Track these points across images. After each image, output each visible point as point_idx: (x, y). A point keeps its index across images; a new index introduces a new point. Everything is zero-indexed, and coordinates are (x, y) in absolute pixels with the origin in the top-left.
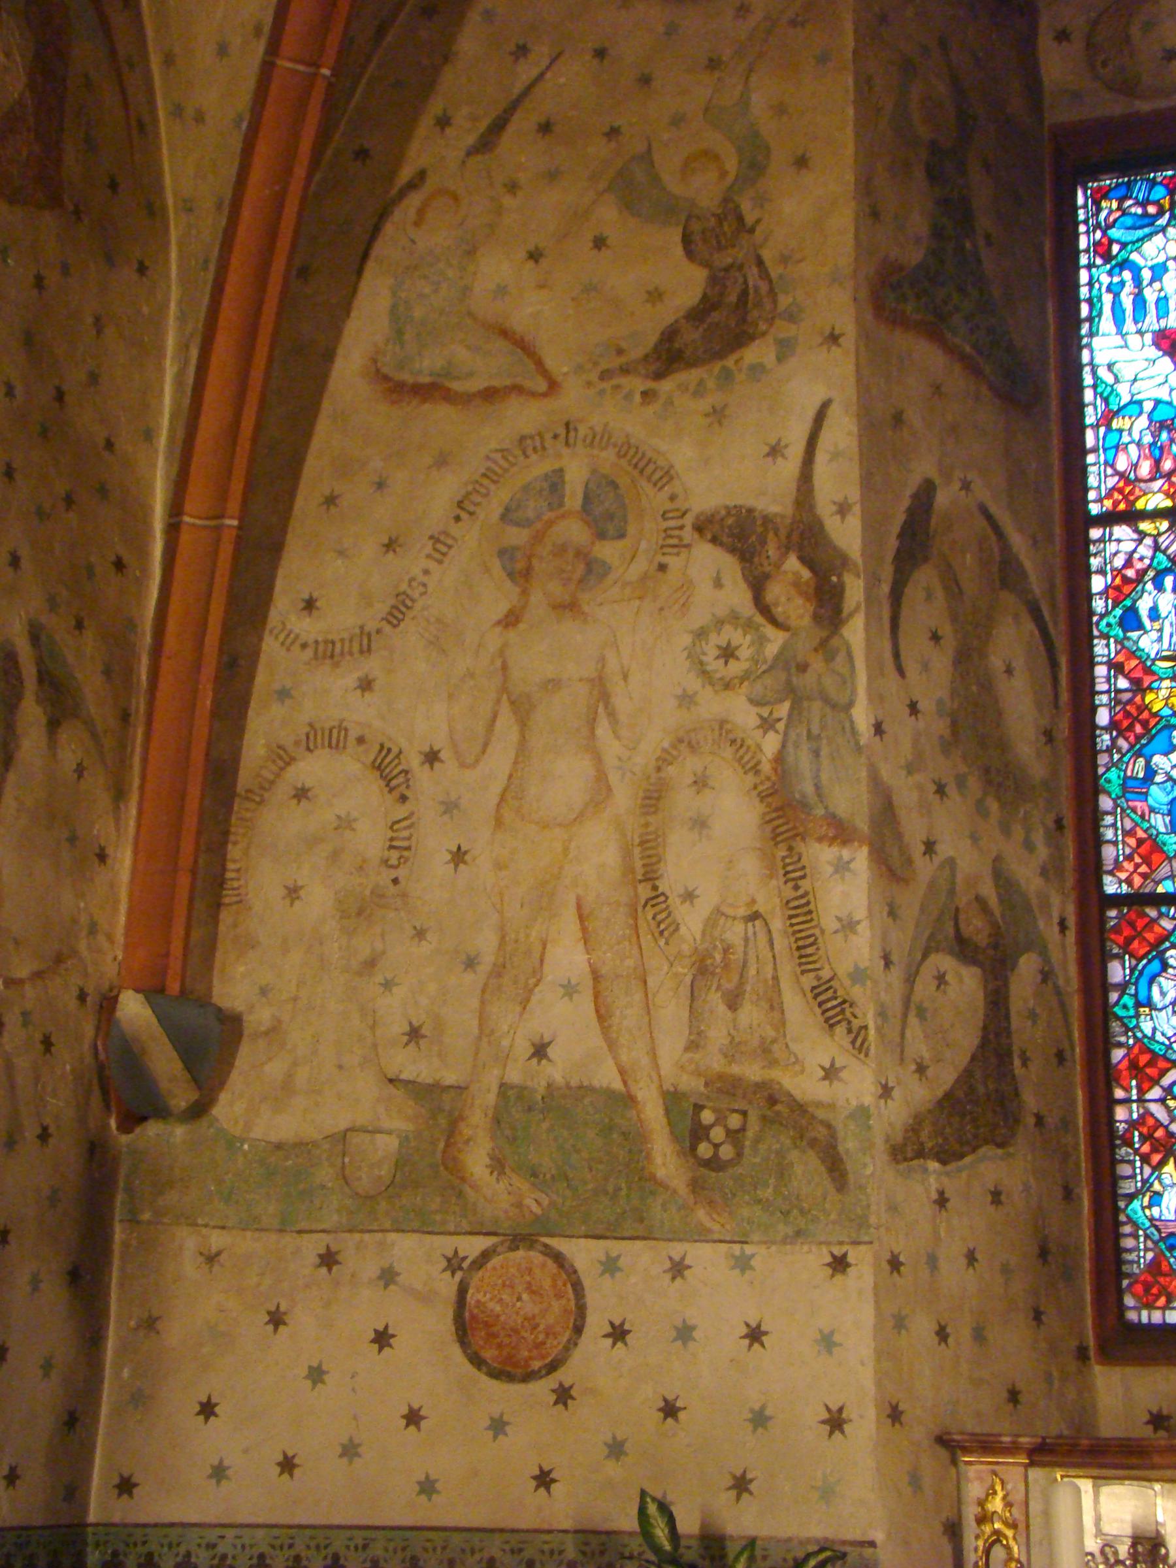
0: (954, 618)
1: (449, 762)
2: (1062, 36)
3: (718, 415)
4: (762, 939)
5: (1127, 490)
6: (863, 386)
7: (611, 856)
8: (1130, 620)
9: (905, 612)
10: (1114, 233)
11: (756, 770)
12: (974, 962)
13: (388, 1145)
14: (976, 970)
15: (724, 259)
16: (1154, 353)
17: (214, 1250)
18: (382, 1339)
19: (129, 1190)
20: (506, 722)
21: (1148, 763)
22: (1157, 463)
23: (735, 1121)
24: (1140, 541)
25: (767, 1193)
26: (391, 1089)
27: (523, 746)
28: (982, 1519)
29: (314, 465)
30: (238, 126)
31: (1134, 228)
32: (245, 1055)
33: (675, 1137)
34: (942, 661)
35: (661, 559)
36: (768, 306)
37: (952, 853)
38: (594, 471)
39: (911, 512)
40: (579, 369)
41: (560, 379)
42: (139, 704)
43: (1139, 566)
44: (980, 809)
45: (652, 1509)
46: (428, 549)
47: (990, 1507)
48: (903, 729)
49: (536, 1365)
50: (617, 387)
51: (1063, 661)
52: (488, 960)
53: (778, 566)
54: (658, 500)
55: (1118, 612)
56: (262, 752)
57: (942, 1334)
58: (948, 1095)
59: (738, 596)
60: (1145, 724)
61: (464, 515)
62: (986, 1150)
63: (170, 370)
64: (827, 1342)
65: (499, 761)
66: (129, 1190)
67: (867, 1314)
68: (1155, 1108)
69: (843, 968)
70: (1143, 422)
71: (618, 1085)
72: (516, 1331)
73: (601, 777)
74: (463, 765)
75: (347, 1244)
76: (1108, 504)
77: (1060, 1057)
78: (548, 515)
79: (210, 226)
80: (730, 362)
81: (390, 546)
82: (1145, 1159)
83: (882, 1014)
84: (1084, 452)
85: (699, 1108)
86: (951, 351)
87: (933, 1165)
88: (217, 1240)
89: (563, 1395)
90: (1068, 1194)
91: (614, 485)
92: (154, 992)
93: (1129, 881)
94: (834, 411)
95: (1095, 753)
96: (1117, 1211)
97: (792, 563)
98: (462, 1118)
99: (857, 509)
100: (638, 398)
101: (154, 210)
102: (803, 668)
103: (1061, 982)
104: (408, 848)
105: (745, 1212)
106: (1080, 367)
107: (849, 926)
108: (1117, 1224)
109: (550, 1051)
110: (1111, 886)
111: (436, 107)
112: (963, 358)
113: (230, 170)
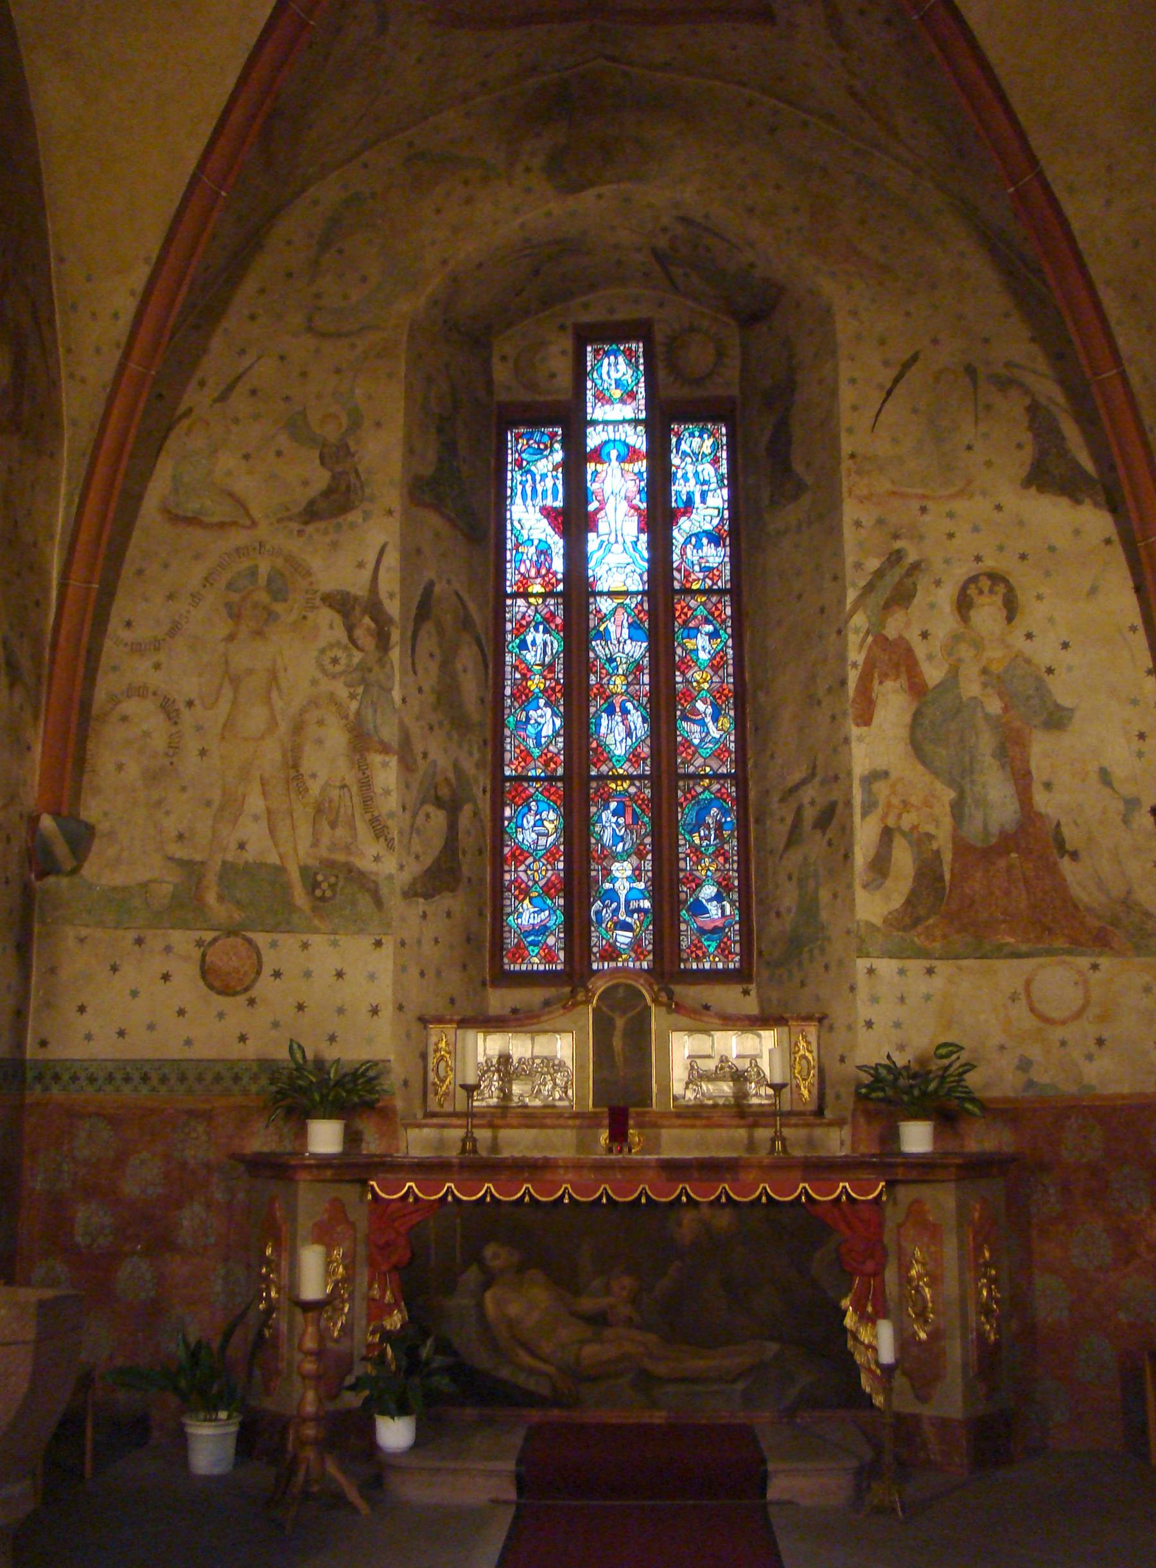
2: (504, 358)
3: (335, 545)
4: (347, 795)
5: (525, 581)
6: (403, 536)
7: (278, 756)
8: (523, 646)
10: (524, 456)
13: (168, 888)
14: (444, 812)
15: (339, 469)
16: (539, 516)
17: (83, 936)
21: (527, 715)
22: (538, 571)
23: (333, 880)
24: (529, 608)
25: (347, 912)
27: (235, 702)
28: (436, 1051)
29: (132, 552)
31: (533, 454)
32: (97, 845)
33: (304, 886)
34: (434, 667)
35: (304, 613)
36: (360, 493)
38: (273, 567)
42: (46, 671)
43: (528, 619)
44: (450, 737)
46: (190, 600)
47: (440, 1046)
49: (239, 989)
51: (491, 666)
52: (216, 804)
53: (360, 621)
55: (517, 641)
56: (104, 696)
57: (422, 974)
59: (340, 634)
60: (527, 696)
61: (208, 585)
63: (62, 504)
64: (372, 977)
65: (224, 706)
67: (390, 966)
69: (384, 810)
70: (532, 550)
71: (278, 862)
72: (229, 974)
73: (273, 717)
76: (515, 588)
77: (480, 852)
80: (340, 520)
82: (516, 897)
83: (401, 833)
84: (506, 562)
85: (316, 874)
86: (442, 514)
87: (421, 900)
88: (84, 932)
89: (252, 1002)
91: (283, 575)
92: (56, 814)
93: (516, 770)
94: (389, 548)
95: (503, 708)
96: (502, 921)
97: (367, 620)
98: (204, 876)
99: (398, 596)
101: (58, 425)
103: (482, 817)
104: (177, 748)
105: (336, 921)
106: (506, 520)
107: (387, 792)
108: (503, 926)
109: (247, 847)
110: (507, 773)
111: (199, 375)
112: (449, 520)
113: (99, 410)
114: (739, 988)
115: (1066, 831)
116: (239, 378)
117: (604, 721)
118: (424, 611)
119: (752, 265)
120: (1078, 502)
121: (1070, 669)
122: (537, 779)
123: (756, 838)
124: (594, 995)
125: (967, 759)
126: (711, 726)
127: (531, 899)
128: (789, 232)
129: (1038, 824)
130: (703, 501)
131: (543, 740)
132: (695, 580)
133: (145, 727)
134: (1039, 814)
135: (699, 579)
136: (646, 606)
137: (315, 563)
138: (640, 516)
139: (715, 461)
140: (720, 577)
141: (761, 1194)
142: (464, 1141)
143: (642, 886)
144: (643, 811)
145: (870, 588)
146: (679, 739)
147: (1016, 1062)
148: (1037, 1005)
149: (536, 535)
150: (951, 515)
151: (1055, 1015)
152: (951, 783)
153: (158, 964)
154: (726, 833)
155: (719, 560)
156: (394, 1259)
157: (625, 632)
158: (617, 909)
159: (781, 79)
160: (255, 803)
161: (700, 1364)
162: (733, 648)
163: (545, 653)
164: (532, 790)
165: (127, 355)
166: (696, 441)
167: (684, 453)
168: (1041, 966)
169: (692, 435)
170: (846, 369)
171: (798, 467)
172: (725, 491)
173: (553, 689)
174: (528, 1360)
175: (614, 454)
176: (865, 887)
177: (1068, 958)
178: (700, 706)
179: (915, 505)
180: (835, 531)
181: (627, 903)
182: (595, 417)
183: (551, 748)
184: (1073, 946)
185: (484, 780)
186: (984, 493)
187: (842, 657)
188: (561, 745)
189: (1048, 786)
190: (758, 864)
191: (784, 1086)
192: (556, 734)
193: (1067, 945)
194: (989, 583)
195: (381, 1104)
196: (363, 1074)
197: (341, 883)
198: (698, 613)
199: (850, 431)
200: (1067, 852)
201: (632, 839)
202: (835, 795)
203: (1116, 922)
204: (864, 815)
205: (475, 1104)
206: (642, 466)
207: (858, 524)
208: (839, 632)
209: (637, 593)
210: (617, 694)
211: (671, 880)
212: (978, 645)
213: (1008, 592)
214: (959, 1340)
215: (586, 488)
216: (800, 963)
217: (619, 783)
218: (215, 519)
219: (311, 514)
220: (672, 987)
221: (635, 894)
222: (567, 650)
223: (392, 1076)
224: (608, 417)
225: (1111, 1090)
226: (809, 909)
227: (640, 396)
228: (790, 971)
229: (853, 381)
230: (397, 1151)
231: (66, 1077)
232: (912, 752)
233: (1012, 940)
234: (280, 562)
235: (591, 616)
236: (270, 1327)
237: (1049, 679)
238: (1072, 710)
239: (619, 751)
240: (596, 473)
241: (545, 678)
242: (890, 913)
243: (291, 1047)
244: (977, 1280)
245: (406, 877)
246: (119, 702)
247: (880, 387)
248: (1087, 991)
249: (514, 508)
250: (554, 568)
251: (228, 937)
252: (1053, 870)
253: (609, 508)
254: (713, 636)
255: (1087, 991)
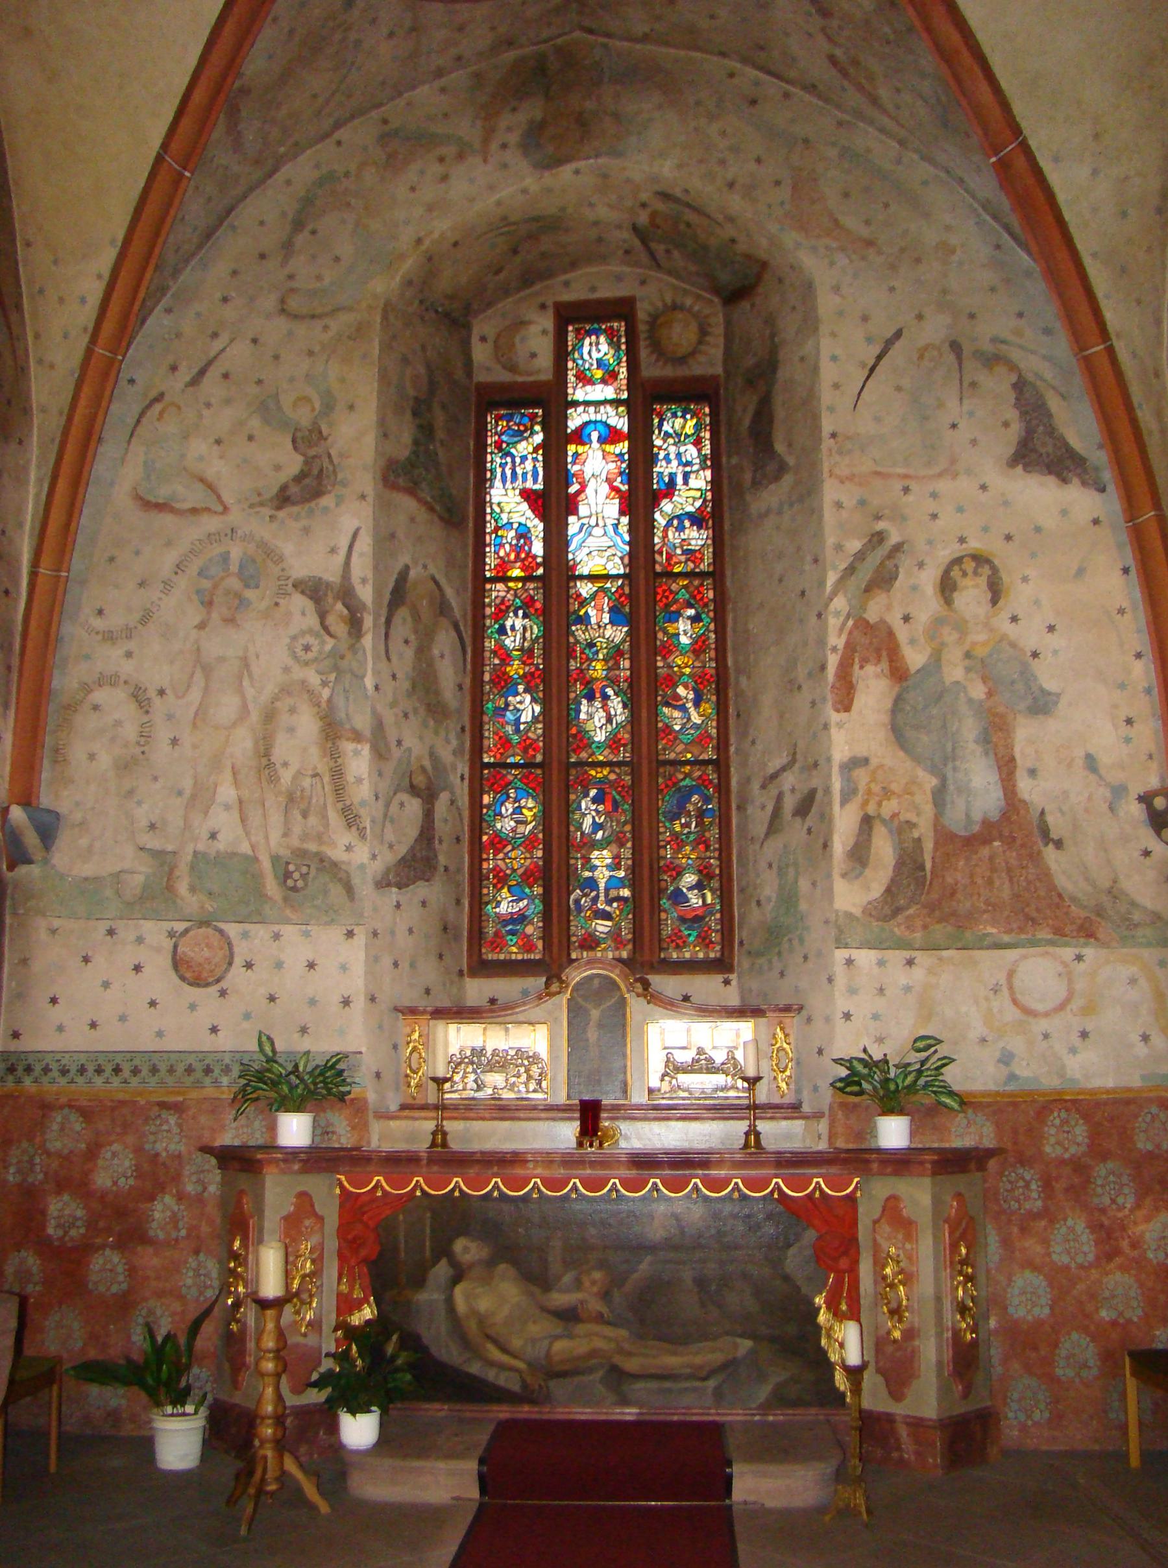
0: (416, 632)
1: (170, 696)
2: (483, 339)
3: (306, 530)
4: (319, 785)
7: (249, 744)
8: (502, 631)
9: (392, 632)
10: (504, 438)
11: (318, 705)
12: (418, 796)
13: (139, 879)
14: (419, 800)
15: (312, 452)
16: (519, 499)
18: (137, 968)
19: (13, 898)
20: (199, 676)
23: (304, 870)
24: (508, 592)
25: (318, 902)
26: (142, 853)
27: (206, 690)
30: (73, 375)
31: (512, 436)
33: (276, 877)
34: (409, 653)
36: (332, 478)
37: (410, 745)
38: (245, 554)
39: (397, 581)
40: (239, 501)
41: (229, 506)
44: (425, 724)
45: (264, 1039)
48: (389, 687)
49: (211, 980)
50: (258, 513)
52: (188, 792)
54: (275, 570)
55: (497, 626)
57: (396, 965)
58: (403, 858)
59: (313, 621)
62: (420, 883)
63: (32, 490)
64: (344, 968)
65: (195, 696)
66: (13, 898)
67: (362, 955)
68: (500, 863)
69: (356, 800)
70: (512, 533)
71: (250, 852)
72: (200, 964)
73: (245, 706)
74: (178, 697)
75: (120, 925)
77: (458, 840)
78: (222, 574)
79: (55, 424)
80: (313, 504)
81: (142, 584)
83: (373, 821)
85: (288, 863)
86: (420, 500)
87: (394, 890)
88: (56, 923)
89: (223, 993)
90: (458, 902)
91: (254, 561)
94: (362, 532)
97: (339, 606)
99: (371, 582)
100: (268, 518)
101: (26, 411)
102: (342, 657)
105: (308, 911)
106: (485, 502)
107: (359, 781)
112: (425, 503)
114: (720, 978)
115: (1050, 819)
116: (210, 363)
117: (584, 708)
118: (398, 595)
119: (733, 241)
120: (1065, 481)
121: (1055, 652)
122: (516, 766)
123: (738, 826)
124: (567, 987)
125: (949, 746)
126: (692, 711)
127: (509, 887)
128: (770, 206)
129: (1022, 812)
130: (686, 483)
131: (522, 727)
132: (676, 563)
133: (117, 716)
134: (1024, 802)
135: (680, 563)
136: (627, 590)
137: (287, 548)
138: (621, 499)
139: (698, 443)
140: (702, 560)
141: (815, 1189)
142: (434, 1134)
143: (622, 874)
144: (623, 797)
145: (851, 570)
146: (660, 725)
147: (998, 1054)
148: (1019, 996)
149: (516, 519)
150: (934, 495)
151: (1040, 1007)
152: (934, 770)
153: (129, 955)
154: (707, 821)
155: (700, 542)
156: (363, 1252)
157: (606, 618)
158: (595, 900)
159: (762, 48)
160: (227, 792)
161: (672, 1361)
162: (716, 632)
163: (524, 639)
164: (510, 778)
165: (94, 340)
166: (679, 422)
167: (666, 433)
168: (1025, 957)
169: (675, 415)
170: (827, 347)
171: (780, 447)
172: (708, 473)
173: (532, 674)
174: (495, 1353)
175: (595, 436)
176: (844, 876)
177: (1051, 949)
178: (681, 691)
179: (898, 486)
180: (815, 512)
181: (607, 890)
182: (575, 398)
183: (530, 735)
184: (1057, 937)
185: (463, 768)
186: (969, 472)
187: (821, 642)
188: (540, 732)
189: (1032, 772)
190: (739, 855)
191: (758, 1079)
192: (535, 719)
193: (1049, 937)
194: (973, 564)
195: (351, 1096)
196: (333, 1067)
197: (313, 872)
198: (679, 596)
199: (831, 409)
200: (1052, 840)
201: (612, 826)
202: (815, 782)
203: (1100, 911)
204: (844, 802)
205: (447, 1096)
206: (623, 447)
207: (839, 505)
208: (819, 615)
209: (618, 576)
210: (597, 679)
211: (651, 868)
212: (961, 627)
213: (993, 574)
214: (933, 1340)
215: (567, 471)
216: (779, 953)
217: (599, 770)
218: (188, 505)
219: (283, 499)
220: (648, 977)
221: (614, 882)
222: (546, 635)
223: (364, 1068)
224: (589, 398)
225: (1096, 1083)
226: (788, 899)
227: (621, 376)
228: (770, 961)
229: (834, 358)
230: (369, 1143)
231: (38, 1068)
232: (893, 738)
233: (994, 931)
234: (251, 548)
235: (571, 601)
236: (238, 1321)
237: (1035, 664)
238: (1058, 695)
239: (600, 737)
240: (576, 455)
241: (524, 663)
242: (869, 903)
243: (260, 1038)
244: (953, 1278)
245: (378, 867)
246: (90, 691)
247: (863, 365)
248: (1070, 981)
249: (493, 492)
250: (534, 551)
251: (200, 927)
252: (1035, 857)
253: (589, 490)
254: (695, 619)
255: (1070, 981)
